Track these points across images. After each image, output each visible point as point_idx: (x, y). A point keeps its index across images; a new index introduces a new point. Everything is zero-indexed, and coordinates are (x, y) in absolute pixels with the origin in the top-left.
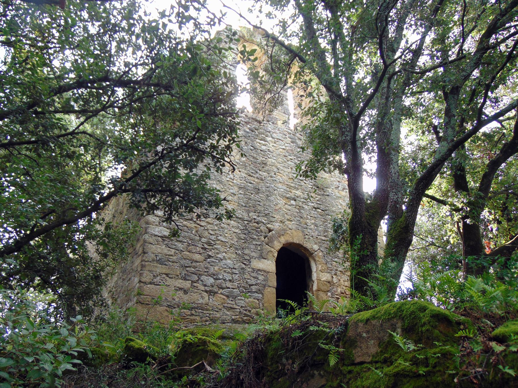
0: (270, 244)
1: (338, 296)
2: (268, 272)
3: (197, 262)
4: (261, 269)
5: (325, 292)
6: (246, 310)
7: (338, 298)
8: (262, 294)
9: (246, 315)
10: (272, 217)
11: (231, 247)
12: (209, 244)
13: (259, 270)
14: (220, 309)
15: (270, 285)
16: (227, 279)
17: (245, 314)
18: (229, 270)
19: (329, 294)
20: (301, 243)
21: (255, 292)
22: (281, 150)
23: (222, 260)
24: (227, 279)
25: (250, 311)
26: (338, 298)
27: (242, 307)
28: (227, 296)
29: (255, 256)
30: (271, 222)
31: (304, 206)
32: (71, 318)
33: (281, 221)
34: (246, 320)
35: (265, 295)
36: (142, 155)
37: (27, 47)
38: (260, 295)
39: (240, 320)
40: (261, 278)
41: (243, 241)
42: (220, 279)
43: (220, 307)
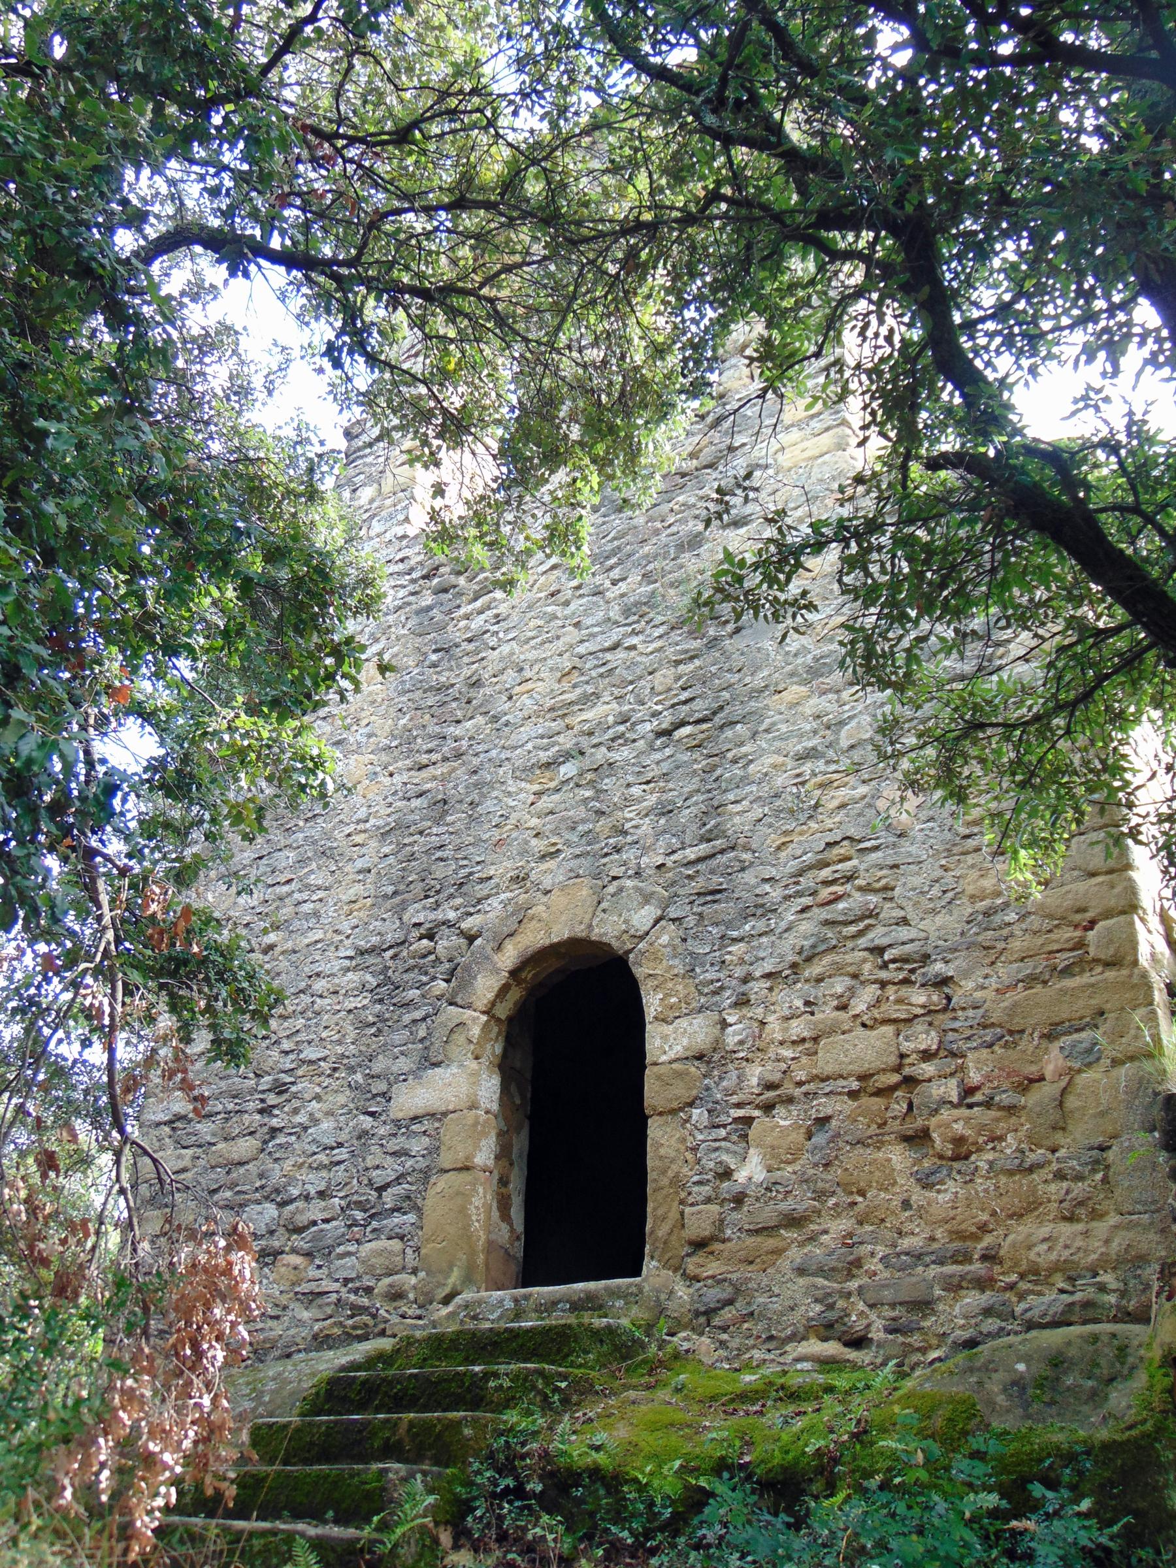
0: (459, 1000)
1: (740, 1113)
2: (445, 1114)
3: (241, 1164)
4: (420, 1112)
5: (673, 1112)
6: (356, 1291)
7: (748, 1121)
8: (418, 1210)
9: (357, 1310)
10: (482, 880)
11: (335, 1069)
12: (280, 1089)
13: (415, 1119)
14: (285, 1308)
15: (447, 1166)
16: (313, 1192)
17: (353, 1307)
18: (322, 1158)
19: (698, 1114)
20: (580, 931)
21: (394, 1210)
22: (543, 579)
23: (306, 1129)
24: (313, 1192)
25: (369, 1290)
26: (748, 1121)
27: (347, 1281)
28: (309, 1255)
29: (406, 1069)
30: (479, 901)
31: (614, 756)
32: (1129, 1519)
33: (516, 879)
34: (354, 1328)
35: (427, 1211)
36: (1120, 329)
37: (207, 601)
38: (411, 1218)
39: (337, 1331)
40: (417, 1146)
41: (373, 1030)
42: (292, 1201)
43: (284, 1299)
